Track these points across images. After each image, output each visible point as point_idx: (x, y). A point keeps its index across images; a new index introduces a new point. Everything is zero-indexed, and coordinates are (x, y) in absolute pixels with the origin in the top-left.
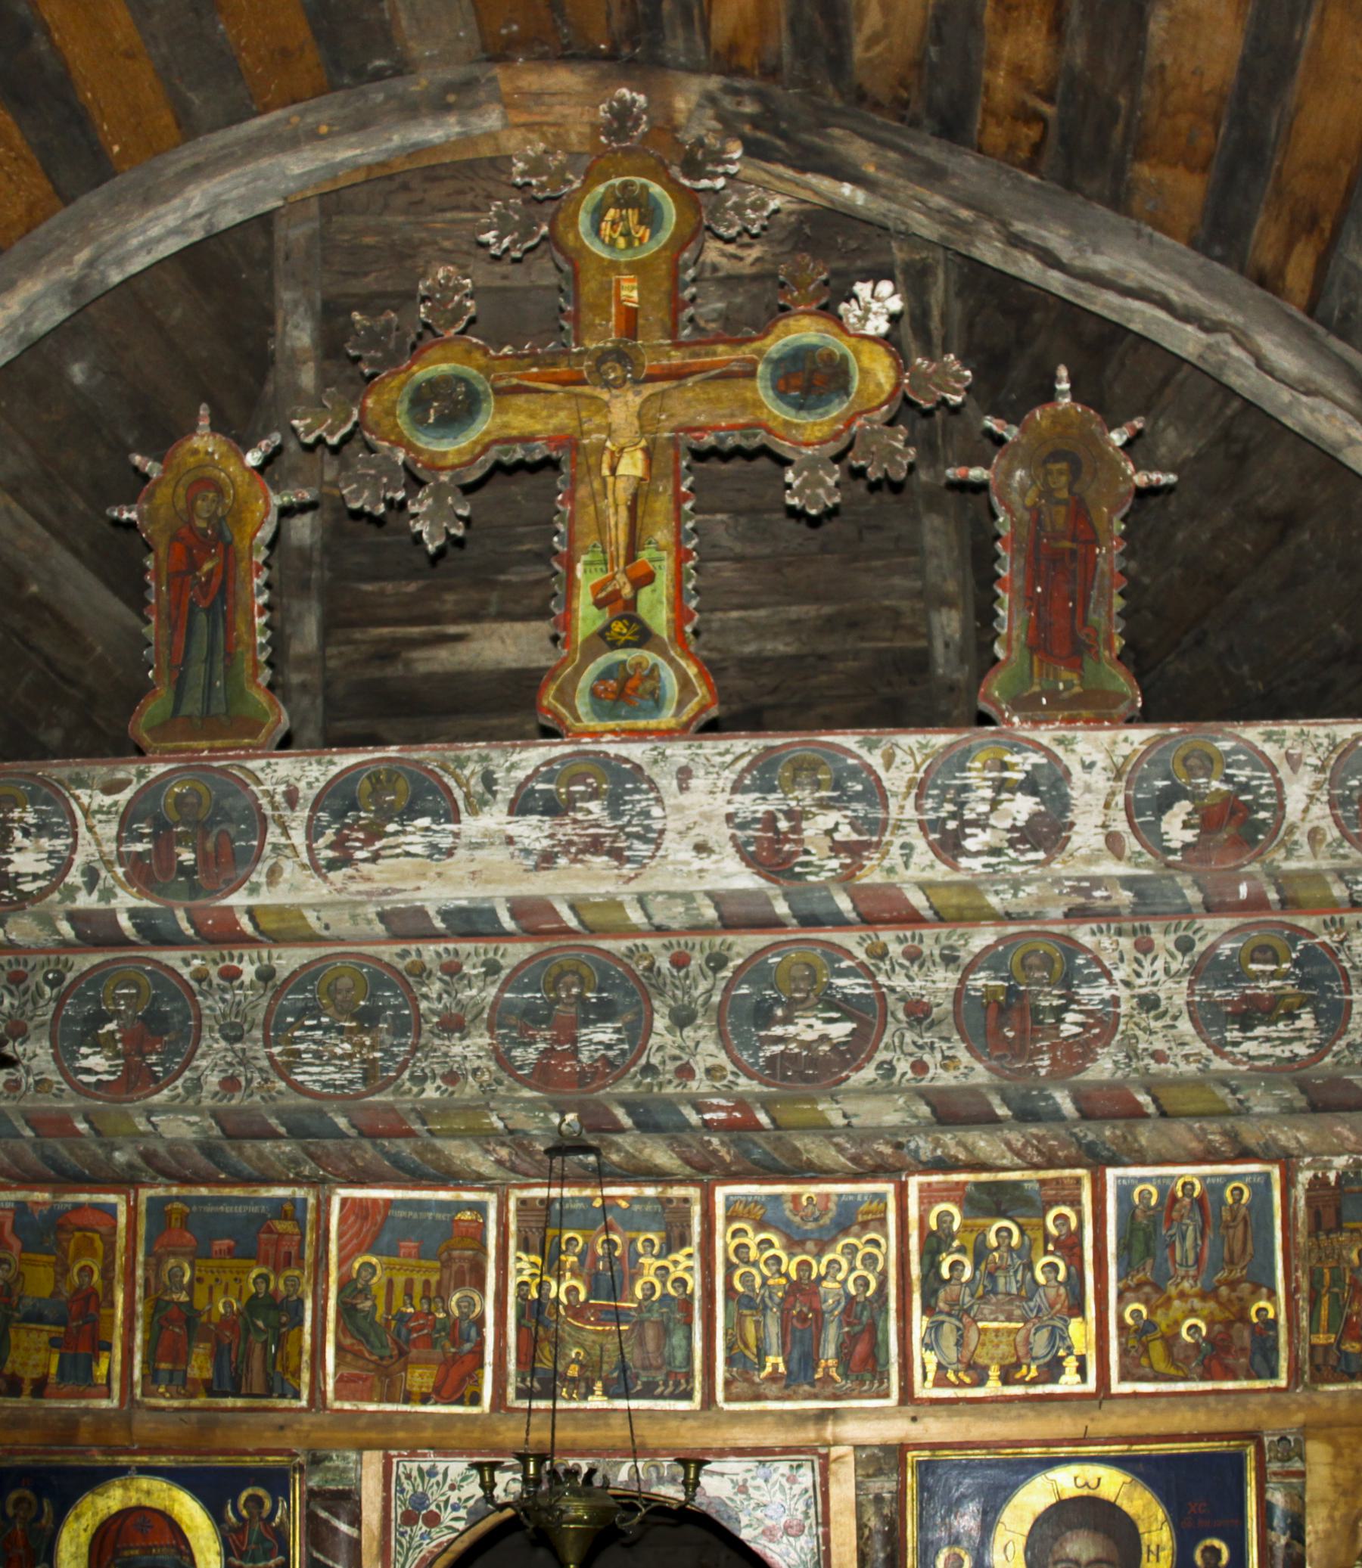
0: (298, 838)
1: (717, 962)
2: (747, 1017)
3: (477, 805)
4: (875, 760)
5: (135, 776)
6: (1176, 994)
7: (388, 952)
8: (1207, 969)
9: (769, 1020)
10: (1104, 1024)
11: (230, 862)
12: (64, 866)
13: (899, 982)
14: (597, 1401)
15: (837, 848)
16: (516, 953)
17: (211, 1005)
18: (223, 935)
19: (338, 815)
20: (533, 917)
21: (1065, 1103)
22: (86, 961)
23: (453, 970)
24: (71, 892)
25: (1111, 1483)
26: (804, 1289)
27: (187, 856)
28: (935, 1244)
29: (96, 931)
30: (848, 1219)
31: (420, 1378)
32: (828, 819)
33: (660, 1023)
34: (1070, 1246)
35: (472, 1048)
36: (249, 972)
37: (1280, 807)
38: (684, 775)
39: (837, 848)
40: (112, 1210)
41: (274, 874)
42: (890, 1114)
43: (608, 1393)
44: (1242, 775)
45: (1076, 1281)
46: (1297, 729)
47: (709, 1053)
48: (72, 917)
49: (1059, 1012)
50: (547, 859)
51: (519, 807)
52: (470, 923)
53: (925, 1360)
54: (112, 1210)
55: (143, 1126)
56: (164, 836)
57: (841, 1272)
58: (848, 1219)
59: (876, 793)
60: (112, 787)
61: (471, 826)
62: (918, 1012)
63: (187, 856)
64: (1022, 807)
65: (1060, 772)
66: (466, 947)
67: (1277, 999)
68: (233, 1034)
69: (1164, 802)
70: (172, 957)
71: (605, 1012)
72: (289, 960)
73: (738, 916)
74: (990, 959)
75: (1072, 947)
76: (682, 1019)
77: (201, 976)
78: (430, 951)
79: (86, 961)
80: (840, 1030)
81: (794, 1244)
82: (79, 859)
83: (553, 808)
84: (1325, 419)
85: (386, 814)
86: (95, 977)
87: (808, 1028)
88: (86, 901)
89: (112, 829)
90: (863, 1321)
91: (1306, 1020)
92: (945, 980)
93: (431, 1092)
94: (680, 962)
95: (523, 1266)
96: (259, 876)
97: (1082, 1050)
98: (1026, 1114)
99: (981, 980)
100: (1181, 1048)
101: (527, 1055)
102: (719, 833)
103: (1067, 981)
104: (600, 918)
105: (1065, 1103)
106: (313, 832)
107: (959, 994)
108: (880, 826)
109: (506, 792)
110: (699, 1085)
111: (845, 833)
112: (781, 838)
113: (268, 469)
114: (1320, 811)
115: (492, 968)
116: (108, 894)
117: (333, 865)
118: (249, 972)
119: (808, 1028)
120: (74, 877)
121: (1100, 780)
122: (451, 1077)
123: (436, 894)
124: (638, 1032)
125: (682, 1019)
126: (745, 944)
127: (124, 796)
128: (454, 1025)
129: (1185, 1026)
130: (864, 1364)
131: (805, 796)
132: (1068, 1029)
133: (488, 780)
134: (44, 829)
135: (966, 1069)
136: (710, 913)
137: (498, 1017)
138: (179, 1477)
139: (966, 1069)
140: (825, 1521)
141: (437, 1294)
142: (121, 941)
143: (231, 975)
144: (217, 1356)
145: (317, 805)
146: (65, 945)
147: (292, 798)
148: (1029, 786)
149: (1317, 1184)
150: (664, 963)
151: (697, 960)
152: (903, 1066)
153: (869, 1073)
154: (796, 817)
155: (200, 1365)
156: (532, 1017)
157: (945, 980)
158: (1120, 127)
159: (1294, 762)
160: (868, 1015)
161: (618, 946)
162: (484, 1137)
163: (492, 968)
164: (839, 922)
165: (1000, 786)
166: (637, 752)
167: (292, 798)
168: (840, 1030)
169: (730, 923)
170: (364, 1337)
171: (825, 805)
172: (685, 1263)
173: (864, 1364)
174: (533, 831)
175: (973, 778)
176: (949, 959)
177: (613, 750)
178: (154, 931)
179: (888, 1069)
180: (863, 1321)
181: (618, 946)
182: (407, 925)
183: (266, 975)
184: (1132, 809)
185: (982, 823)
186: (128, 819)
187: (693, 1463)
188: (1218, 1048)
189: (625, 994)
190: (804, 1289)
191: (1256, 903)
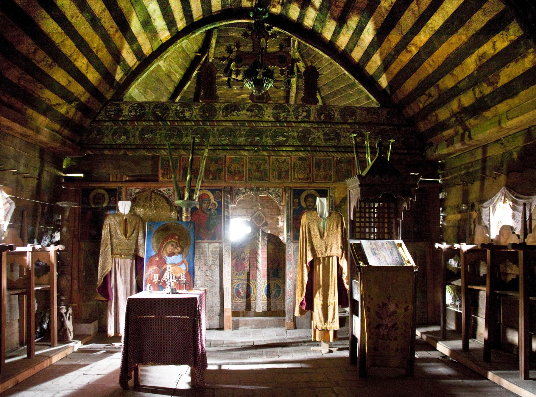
0: (221, 113)
1: (271, 130)
3: (243, 110)
4: (289, 107)
6: (322, 137)
8: (325, 134)
9: (276, 137)
10: (314, 139)
12: (192, 115)
13: (291, 134)
15: (284, 117)
17: (211, 133)
19: (226, 110)
23: (240, 130)
27: (207, 115)
32: (283, 114)
37: (334, 116)
38: (267, 108)
39: (284, 117)
44: (330, 112)
45: (310, 171)
49: (309, 138)
50: (251, 117)
51: (248, 111)
56: (204, 112)
59: (289, 111)
61: (242, 112)
62: (293, 137)
63: (207, 115)
64: (305, 114)
67: (333, 138)
68: (214, 137)
69: (321, 114)
71: (258, 136)
74: (301, 131)
75: (311, 131)
76: (266, 137)
77: (210, 130)
80: (284, 139)
83: (251, 111)
85: (231, 111)
86: (197, 129)
87: (281, 139)
89: (198, 111)
91: (336, 141)
92: (296, 134)
95: (248, 165)
99: (300, 134)
100: (322, 143)
102: (271, 115)
103: (310, 134)
106: (223, 112)
107: (298, 135)
108: (289, 115)
109: (246, 109)
111: (285, 116)
112: (278, 116)
113: (10, 256)
114: (339, 116)
115: (245, 130)
117: (225, 116)
119: (281, 139)
120: (193, 117)
121: (314, 111)
124: (262, 138)
125: (266, 137)
129: (323, 140)
131: (280, 111)
132: (310, 140)
133: (244, 107)
134: (189, 111)
137: (246, 135)
138: (209, 190)
143: (213, 129)
144: (213, 175)
145: (223, 109)
146: (193, 125)
147: (220, 108)
148: (306, 111)
149: (337, 160)
150: (264, 130)
151: (268, 130)
154: (279, 113)
155: (211, 177)
156: (250, 136)
157: (296, 134)
158: (529, 101)
159: (336, 110)
160: (287, 137)
163: (245, 130)
165: (303, 111)
166: (262, 105)
167: (220, 108)
168: (284, 139)
170: (230, 173)
171: (283, 112)
174: (248, 113)
175: (300, 110)
176: (297, 131)
177: (258, 104)
183: (218, 130)
184: (318, 115)
185: (301, 115)
188: (326, 143)
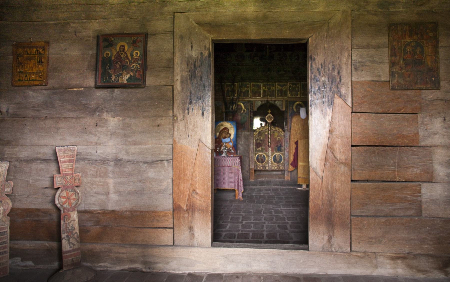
25: (301, 103)
26: (282, 90)
28: (290, 87)
31: (257, 95)
34: (298, 87)
46: (253, 268)
53: (289, 95)
57: (284, 88)
58: (284, 85)
64: (296, 57)
65: (216, 191)
81: (281, 87)
84: (203, 280)
90: (285, 92)
95: (264, 88)
130: (285, 95)
141: (258, 90)
172: (274, 88)
173: (285, 95)
187: (275, 101)
190: (282, 90)
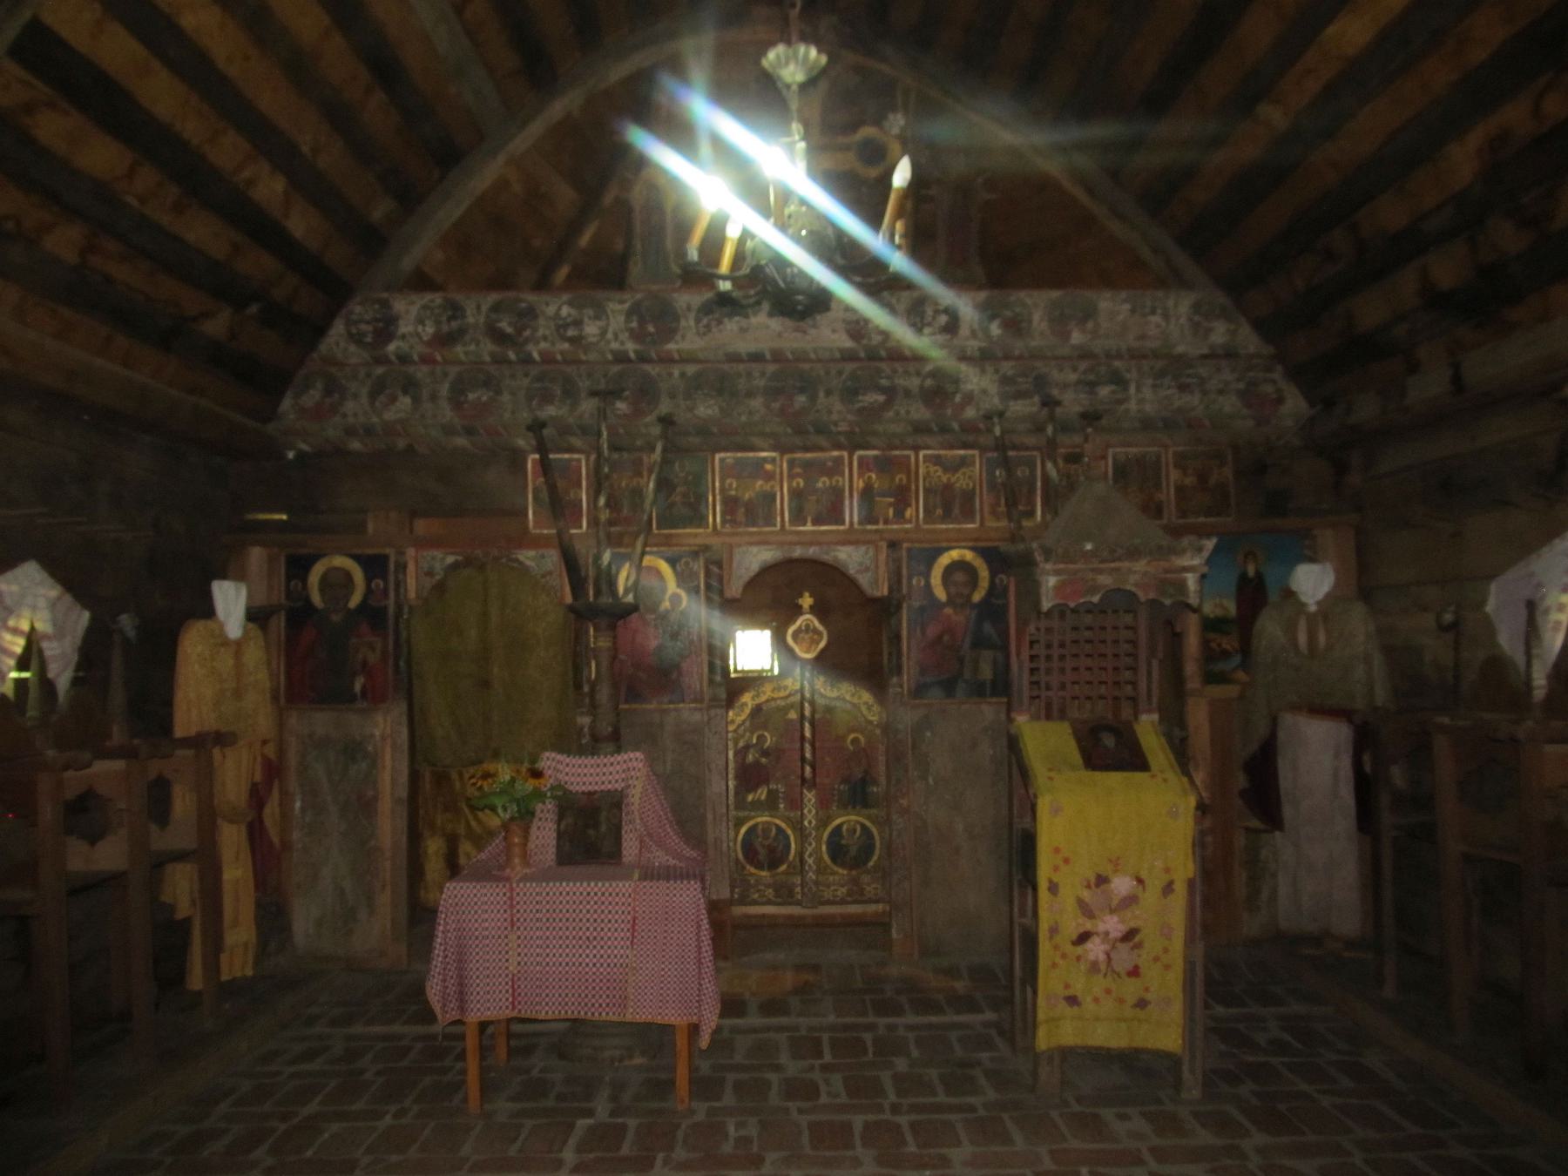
0: (692, 323)
2: (850, 394)
5: (629, 299)
7: (726, 367)
11: (669, 333)
14: (809, 527)
16: (771, 368)
18: (668, 360)
20: (778, 356)
21: (956, 426)
22: (616, 369)
23: (749, 374)
24: (609, 342)
25: (969, 555)
29: (621, 358)
30: (963, 462)
33: (822, 394)
35: (757, 403)
36: (676, 373)
40: (908, 457)
41: (683, 337)
42: (898, 428)
43: (814, 524)
44: (1018, 310)
47: (838, 406)
48: (612, 351)
49: (954, 393)
52: (757, 358)
54: (908, 457)
55: (644, 430)
56: (642, 322)
57: (961, 481)
60: (622, 302)
61: (754, 320)
62: (907, 393)
66: (754, 365)
68: (673, 396)
70: (647, 367)
71: (802, 390)
72: (691, 369)
73: (848, 356)
76: (828, 393)
78: (741, 367)
79: (616, 369)
82: (611, 330)
88: (615, 346)
90: (968, 496)
93: (744, 418)
94: (828, 373)
96: (678, 337)
97: (962, 406)
98: (944, 429)
99: (929, 382)
101: (776, 405)
104: (801, 357)
105: (956, 426)
106: (698, 321)
107: (921, 387)
110: (835, 417)
115: (763, 374)
116: (622, 343)
118: (676, 373)
120: (610, 336)
122: (750, 413)
123: (744, 346)
125: (828, 393)
126: (849, 367)
127: (627, 306)
128: (750, 394)
134: (597, 318)
135: (920, 412)
136: (610, 357)
139: (920, 412)
140: (877, 567)
142: (629, 361)
143: (670, 375)
145: (699, 311)
147: (689, 308)
152: (903, 412)
153: (891, 414)
160: (891, 392)
161: (806, 366)
162: (762, 434)
163: (763, 374)
164: (881, 359)
167: (689, 308)
169: (844, 359)
176: (918, 374)
178: (642, 358)
179: (898, 413)
180: (968, 496)
181: (806, 366)
182: (734, 358)
183: (683, 375)
186: (629, 314)
189: (808, 385)
191: (1020, 358)
